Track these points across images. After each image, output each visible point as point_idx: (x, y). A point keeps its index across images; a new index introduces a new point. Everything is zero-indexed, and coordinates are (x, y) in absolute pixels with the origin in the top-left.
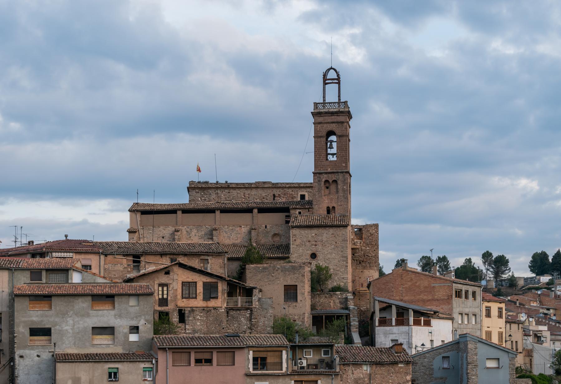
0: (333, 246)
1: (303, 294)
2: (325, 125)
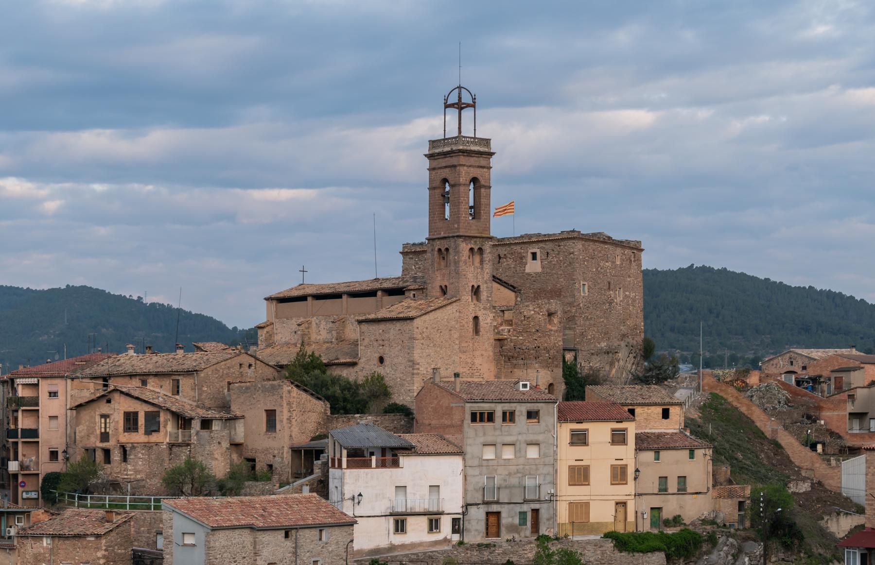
0: (400, 347)
1: (282, 421)
2: (439, 171)
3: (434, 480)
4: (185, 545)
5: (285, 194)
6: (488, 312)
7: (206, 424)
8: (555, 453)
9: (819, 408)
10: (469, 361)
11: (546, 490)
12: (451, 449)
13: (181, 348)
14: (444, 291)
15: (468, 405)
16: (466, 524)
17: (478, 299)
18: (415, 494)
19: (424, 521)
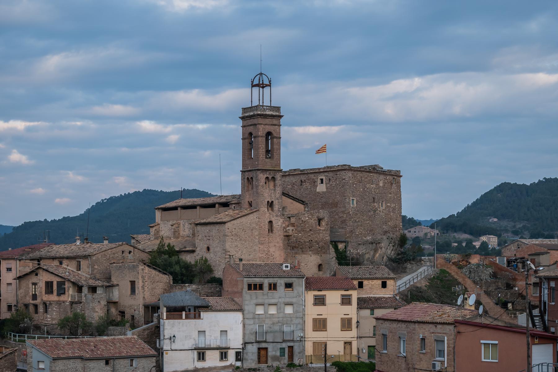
1: (138, 288)
2: (248, 128)
3: (225, 327)
4: (40, 369)
5: (313, 130)
6: (279, 218)
7: (93, 289)
8: (304, 310)
9: (515, 279)
10: (266, 249)
11: (299, 334)
12: (235, 307)
13: (107, 239)
14: (250, 204)
15: (245, 279)
16: (245, 355)
17: (272, 210)
18: (211, 336)
19: (217, 354)
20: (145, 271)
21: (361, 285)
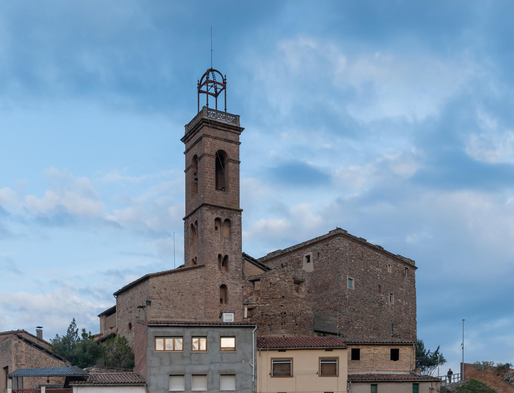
8: (254, 384)
17: (227, 270)
20: (19, 348)
21: (355, 355)
